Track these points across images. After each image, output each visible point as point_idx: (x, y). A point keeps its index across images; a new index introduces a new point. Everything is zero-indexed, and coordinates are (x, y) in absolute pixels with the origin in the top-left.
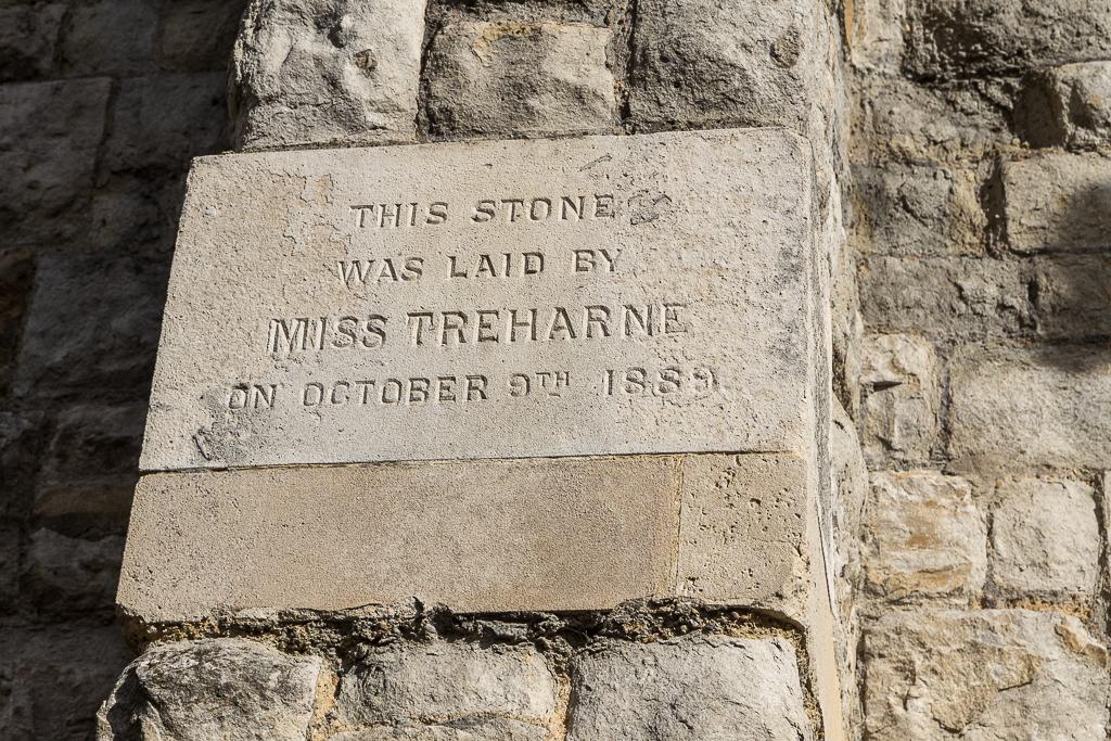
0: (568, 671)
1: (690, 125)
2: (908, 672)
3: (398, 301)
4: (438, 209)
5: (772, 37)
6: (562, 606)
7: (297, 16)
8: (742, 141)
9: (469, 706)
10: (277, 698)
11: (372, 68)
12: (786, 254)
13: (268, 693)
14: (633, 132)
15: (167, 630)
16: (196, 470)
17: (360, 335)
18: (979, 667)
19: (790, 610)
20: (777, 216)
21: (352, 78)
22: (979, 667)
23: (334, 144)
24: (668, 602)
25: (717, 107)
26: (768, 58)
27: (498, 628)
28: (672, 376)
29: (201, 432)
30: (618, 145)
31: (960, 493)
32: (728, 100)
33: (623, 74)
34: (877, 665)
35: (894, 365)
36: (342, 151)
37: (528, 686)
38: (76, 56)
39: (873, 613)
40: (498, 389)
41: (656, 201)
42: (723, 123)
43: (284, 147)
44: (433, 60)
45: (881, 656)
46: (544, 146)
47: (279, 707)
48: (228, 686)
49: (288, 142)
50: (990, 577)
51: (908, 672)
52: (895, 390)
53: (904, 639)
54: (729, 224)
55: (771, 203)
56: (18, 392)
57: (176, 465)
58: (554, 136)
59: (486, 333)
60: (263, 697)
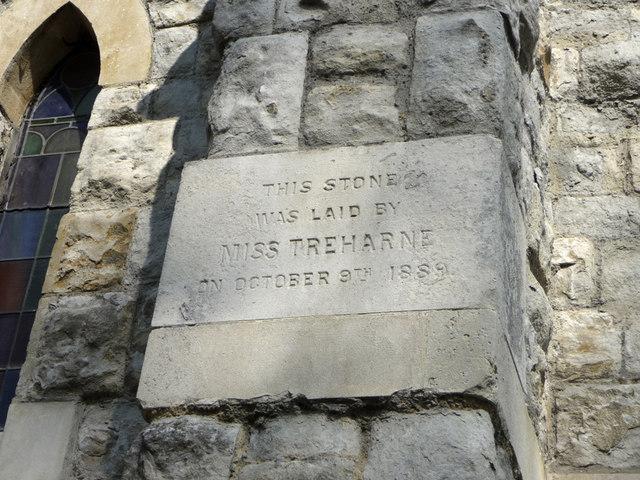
0: (365, 429)
1: (438, 135)
2: (578, 419)
3: (284, 233)
4: (306, 184)
5: (481, 87)
6: (363, 395)
7: (239, 87)
8: (466, 141)
9: (315, 451)
10: (215, 448)
11: (276, 113)
12: (486, 202)
13: (210, 445)
14: (408, 140)
15: (162, 411)
16: (179, 326)
17: (265, 252)
18: (618, 417)
19: (486, 395)
20: (482, 181)
21: (265, 117)
22: (618, 417)
23: (256, 152)
24: (419, 391)
25: (452, 124)
26: (479, 98)
27: (332, 407)
28: (424, 269)
29: (184, 306)
30: (400, 147)
31: (607, 322)
32: (457, 120)
33: (403, 109)
34: (562, 415)
35: (571, 254)
36: (260, 156)
37: (343, 437)
38: (160, 110)
39: (560, 387)
40: (334, 278)
41: (418, 176)
42: (457, 133)
43: (232, 155)
44: (307, 109)
45: (565, 411)
46: (362, 150)
47: (216, 453)
48: (189, 443)
49: (234, 152)
50: (623, 367)
51: (578, 419)
52: (572, 268)
53: (577, 401)
54: (457, 187)
55: (479, 174)
56: (127, 282)
57: (170, 323)
58: (367, 144)
59: (330, 249)
60: (208, 447)
